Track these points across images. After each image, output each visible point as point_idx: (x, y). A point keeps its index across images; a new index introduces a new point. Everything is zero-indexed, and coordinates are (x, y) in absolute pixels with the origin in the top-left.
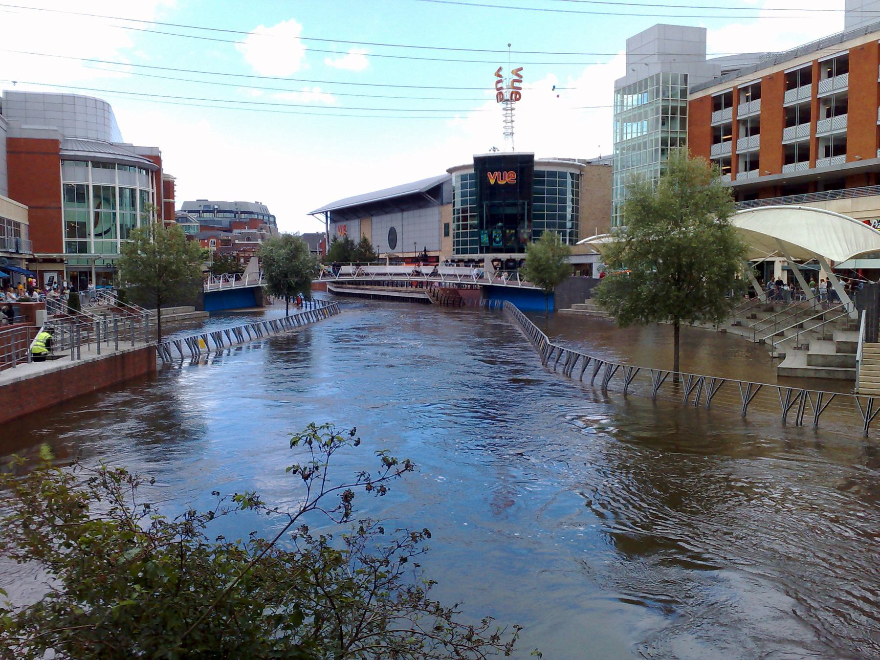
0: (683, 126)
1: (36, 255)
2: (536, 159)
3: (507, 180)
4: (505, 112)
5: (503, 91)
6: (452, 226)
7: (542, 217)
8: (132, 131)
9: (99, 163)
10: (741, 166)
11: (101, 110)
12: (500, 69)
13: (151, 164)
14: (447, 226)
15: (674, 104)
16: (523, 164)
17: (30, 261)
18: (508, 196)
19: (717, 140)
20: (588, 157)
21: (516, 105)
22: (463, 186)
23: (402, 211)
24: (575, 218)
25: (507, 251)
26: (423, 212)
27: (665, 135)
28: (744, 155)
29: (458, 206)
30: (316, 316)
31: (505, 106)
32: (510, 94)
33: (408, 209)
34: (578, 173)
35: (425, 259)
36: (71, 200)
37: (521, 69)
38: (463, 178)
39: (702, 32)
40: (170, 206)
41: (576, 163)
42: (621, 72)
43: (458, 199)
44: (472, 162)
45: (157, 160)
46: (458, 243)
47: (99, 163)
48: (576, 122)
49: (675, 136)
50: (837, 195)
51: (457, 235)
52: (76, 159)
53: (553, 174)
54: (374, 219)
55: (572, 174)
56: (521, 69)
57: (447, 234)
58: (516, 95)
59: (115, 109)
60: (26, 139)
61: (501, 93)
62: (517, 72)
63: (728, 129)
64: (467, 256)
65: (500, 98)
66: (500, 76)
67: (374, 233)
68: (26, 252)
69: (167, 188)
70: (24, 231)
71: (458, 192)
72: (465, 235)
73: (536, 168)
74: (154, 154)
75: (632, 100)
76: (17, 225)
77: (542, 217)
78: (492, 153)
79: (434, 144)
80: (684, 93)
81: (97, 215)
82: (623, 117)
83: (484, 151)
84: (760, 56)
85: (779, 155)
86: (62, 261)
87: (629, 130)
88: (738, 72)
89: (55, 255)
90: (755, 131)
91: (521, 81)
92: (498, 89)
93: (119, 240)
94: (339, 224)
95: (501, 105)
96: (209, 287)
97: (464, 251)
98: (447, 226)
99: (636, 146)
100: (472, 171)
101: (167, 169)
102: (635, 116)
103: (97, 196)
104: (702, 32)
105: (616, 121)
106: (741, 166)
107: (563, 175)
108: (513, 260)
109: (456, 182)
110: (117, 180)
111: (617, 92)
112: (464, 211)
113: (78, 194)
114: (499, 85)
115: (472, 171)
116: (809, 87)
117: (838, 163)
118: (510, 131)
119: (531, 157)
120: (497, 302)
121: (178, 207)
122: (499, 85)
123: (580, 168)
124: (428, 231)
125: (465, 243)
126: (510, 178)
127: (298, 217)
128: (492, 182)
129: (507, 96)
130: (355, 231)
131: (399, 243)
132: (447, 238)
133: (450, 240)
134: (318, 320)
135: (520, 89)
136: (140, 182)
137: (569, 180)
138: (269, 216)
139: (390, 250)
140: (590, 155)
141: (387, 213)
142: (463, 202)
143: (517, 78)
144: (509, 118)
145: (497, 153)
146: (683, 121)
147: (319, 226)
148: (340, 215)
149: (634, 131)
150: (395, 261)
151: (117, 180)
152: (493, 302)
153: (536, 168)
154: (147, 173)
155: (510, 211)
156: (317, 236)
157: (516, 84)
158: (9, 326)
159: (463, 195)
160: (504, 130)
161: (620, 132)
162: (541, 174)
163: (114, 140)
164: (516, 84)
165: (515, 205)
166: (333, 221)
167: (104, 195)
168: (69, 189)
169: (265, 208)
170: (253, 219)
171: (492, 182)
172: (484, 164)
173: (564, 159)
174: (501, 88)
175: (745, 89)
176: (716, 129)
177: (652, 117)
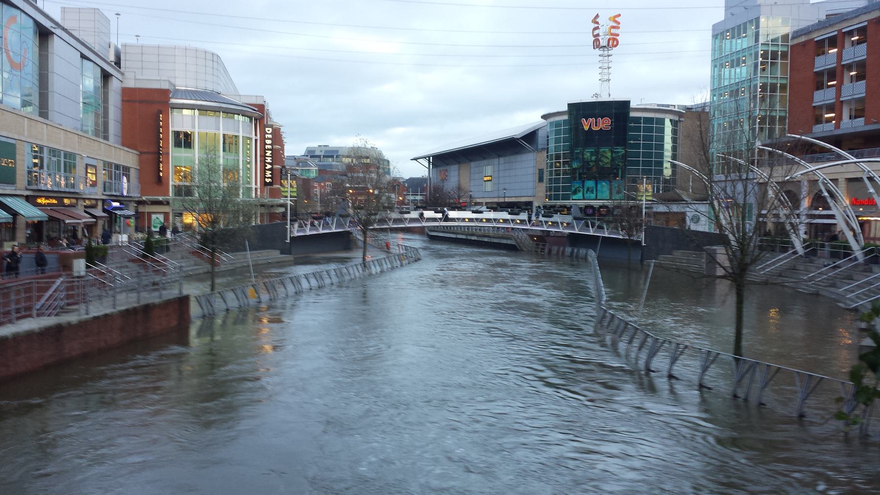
0: (784, 72)
1: (144, 198)
2: (633, 105)
3: (601, 126)
4: (601, 58)
5: (600, 38)
7: (637, 163)
12: (597, 16)
14: (541, 172)
15: (775, 49)
16: (619, 110)
19: (820, 86)
22: (557, 132)
23: (499, 156)
26: (519, 157)
27: (764, 81)
28: (849, 102)
30: (401, 260)
31: (601, 53)
32: (606, 42)
36: (178, 144)
37: (619, 15)
38: (558, 124)
40: (277, 154)
41: (676, 109)
42: (719, 15)
43: (552, 145)
44: (566, 108)
45: (261, 108)
46: (550, 189)
49: (774, 81)
50: (821, 158)
51: (550, 180)
54: (473, 164)
56: (619, 15)
57: (541, 180)
58: (613, 42)
60: (139, 89)
61: (598, 40)
63: (832, 74)
65: (596, 44)
66: (597, 23)
71: (552, 137)
72: (557, 181)
73: (632, 114)
74: (260, 102)
77: (637, 163)
78: (594, 100)
86: (168, 203)
87: (727, 76)
89: (161, 198)
91: (619, 28)
92: (595, 36)
94: (439, 169)
95: (598, 51)
96: (295, 231)
97: (557, 198)
100: (566, 117)
101: (276, 117)
108: (592, 207)
110: (222, 126)
111: (715, 36)
112: (558, 157)
114: (596, 32)
118: (606, 77)
119: (627, 103)
120: (582, 251)
122: (596, 32)
124: (524, 178)
125: (557, 189)
126: (604, 124)
128: (586, 128)
129: (603, 42)
130: (454, 177)
132: (540, 184)
133: (544, 185)
134: (402, 265)
135: (618, 35)
136: (242, 127)
138: (385, 160)
141: (484, 159)
143: (615, 25)
144: (606, 65)
145: (600, 100)
147: (421, 170)
148: (440, 160)
152: (578, 251)
154: (251, 121)
157: (613, 31)
158: (40, 275)
159: (557, 141)
160: (599, 77)
161: (716, 78)
164: (613, 31)
166: (435, 166)
168: (177, 134)
169: (380, 154)
170: (369, 164)
171: (586, 128)
172: (578, 110)
173: (663, 105)
174: (598, 35)
175: (851, 33)
176: (820, 74)
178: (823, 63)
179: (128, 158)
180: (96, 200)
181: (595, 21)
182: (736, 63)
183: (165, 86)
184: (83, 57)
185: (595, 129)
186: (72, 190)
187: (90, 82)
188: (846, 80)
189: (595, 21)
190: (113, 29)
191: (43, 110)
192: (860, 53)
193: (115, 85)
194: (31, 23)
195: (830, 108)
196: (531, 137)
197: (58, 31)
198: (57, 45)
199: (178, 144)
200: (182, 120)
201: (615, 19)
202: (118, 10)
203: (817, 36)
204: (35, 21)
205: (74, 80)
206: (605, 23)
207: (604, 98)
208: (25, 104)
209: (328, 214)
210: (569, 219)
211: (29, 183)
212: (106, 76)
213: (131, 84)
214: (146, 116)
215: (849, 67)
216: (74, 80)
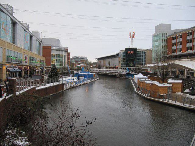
0: (166, 43)
6: (121, 61)
7: (138, 60)
8: (64, 44)
9: (58, 50)
10: (178, 51)
11: (58, 41)
13: (66, 50)
14: (120, 61)
16: (135, 50)
17: (45, 67)
18: (132, 57)
19: (173, 46)
20: (148, 49)
21: (133, 39)
22: (123, 54)
24: (145, 60)
25: (131, 66)
26: (115, 59)
28: (179, 49)
29: (122, 57)
33: (113, 58)
34: (144, 52)
35: (115, 68)
36: (52, 57)
38: (123, 52)
39: (170, 25)
40: (69, 58)
43: (122, 56)
45: (67, 49)
47: (58, 50)
48: (145, 42)
52: (53, 49)
53: (140, 52)
55: (144, 52)
57: (120, 63)
58: (133, 37)
59: (61, 41)
62: (134, 33)
63: (175, 44)
64: (124, 67)
65: (130, 37)
67: (98, 81)
68: (45, 66)
69: (69, 54)
70: (45, 62)
71: (122, 55)
73: (137, 51)
75: (156, 38)
76: (44, 61)
79: (117, 46)
80: (166, 37)
81: (57, 59)
82: (154, 41)
83: (127, 47)
84: (182, 29)
85: (186, 49)
88: (177, 33)
90: (181, 44)
93: (60, 64)
95: (131, 39)
97: (123, 66)
98: (120, 61)
99: (157, 46)
100: (125, 51)
101: (69, 51)
102: (157, 41)
103: (57, 56)
104: (170, 25)
105: (153, 41)
106: (178, 51)
107: (143, 52)
109: (122, 53)
110: (60, 53)
111: (153, 36)
112: (123, 58)
113: (54, 56)
115: (125, 51)
116: (176, 40)
117: (181, 53)
121: (71, 57)
123: (146, 51)
124: (116, 62)
126: (132, 52)
127: (93, 59)
131: (111, 64)
133: (120, 64)
136: (64, 54)
137: (144, 53)
139: (109, 66)
140: (148, 48)
142: (123, 57)
146: (166, 42)
147: (96, 61)
148: (99, 59)
149: (156, 44)
150: (110, 68)
151: (60, 53)
153: (137, 51)
155: (132, 59)
156: (96, 63)
159: (123, 55)
162: (138, 52)
163: (60, 46)
165: (133, 57)
167: (58, 56)
168: (52, 55)
172: (127, 50)
175: (179, 36)
176: (173, 44)
177: (160, 41)
178: (188, 38)
179: (44, 59)
180: (28, 66)
181: (130, 33)
182: (157, 41)
183: (50, 46)
184: (37, 41)
185: (130, 53)
186: (20, 63)
187: (38, 44)
188: (178, 44)
189: (130, 33)
190: (41, 35)
191: (31, 50)
192: (181, 40)
193: (42, 46)
194: (29, 35)
195: (175, 50)
196: (118, 55)
197: (33, 36)
198: (33, 38)
199: (52, 57)
200: (53, 52)
201: (134, 33)
202: (42, 32)
203: (172, 36)
204: (11, 18)
205: (36, 44)
206: (132, 34)
207: (132, 47)
208: (28, 50)
209: (167, 98)
210: (126, 70)
211: (7, 61)
212: (40, 44)
213: (44, 45)
214: (46, 51)
215: (179, 42)
216: (36, 44)
